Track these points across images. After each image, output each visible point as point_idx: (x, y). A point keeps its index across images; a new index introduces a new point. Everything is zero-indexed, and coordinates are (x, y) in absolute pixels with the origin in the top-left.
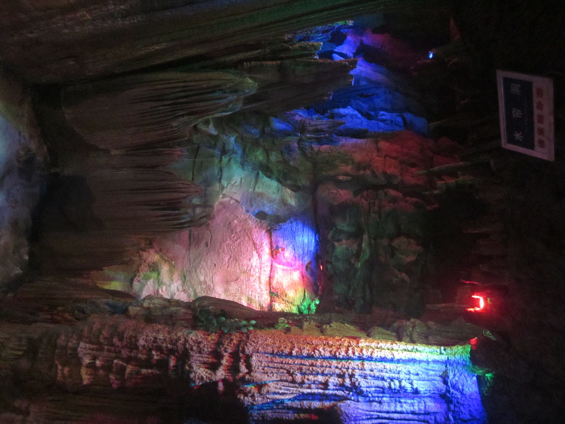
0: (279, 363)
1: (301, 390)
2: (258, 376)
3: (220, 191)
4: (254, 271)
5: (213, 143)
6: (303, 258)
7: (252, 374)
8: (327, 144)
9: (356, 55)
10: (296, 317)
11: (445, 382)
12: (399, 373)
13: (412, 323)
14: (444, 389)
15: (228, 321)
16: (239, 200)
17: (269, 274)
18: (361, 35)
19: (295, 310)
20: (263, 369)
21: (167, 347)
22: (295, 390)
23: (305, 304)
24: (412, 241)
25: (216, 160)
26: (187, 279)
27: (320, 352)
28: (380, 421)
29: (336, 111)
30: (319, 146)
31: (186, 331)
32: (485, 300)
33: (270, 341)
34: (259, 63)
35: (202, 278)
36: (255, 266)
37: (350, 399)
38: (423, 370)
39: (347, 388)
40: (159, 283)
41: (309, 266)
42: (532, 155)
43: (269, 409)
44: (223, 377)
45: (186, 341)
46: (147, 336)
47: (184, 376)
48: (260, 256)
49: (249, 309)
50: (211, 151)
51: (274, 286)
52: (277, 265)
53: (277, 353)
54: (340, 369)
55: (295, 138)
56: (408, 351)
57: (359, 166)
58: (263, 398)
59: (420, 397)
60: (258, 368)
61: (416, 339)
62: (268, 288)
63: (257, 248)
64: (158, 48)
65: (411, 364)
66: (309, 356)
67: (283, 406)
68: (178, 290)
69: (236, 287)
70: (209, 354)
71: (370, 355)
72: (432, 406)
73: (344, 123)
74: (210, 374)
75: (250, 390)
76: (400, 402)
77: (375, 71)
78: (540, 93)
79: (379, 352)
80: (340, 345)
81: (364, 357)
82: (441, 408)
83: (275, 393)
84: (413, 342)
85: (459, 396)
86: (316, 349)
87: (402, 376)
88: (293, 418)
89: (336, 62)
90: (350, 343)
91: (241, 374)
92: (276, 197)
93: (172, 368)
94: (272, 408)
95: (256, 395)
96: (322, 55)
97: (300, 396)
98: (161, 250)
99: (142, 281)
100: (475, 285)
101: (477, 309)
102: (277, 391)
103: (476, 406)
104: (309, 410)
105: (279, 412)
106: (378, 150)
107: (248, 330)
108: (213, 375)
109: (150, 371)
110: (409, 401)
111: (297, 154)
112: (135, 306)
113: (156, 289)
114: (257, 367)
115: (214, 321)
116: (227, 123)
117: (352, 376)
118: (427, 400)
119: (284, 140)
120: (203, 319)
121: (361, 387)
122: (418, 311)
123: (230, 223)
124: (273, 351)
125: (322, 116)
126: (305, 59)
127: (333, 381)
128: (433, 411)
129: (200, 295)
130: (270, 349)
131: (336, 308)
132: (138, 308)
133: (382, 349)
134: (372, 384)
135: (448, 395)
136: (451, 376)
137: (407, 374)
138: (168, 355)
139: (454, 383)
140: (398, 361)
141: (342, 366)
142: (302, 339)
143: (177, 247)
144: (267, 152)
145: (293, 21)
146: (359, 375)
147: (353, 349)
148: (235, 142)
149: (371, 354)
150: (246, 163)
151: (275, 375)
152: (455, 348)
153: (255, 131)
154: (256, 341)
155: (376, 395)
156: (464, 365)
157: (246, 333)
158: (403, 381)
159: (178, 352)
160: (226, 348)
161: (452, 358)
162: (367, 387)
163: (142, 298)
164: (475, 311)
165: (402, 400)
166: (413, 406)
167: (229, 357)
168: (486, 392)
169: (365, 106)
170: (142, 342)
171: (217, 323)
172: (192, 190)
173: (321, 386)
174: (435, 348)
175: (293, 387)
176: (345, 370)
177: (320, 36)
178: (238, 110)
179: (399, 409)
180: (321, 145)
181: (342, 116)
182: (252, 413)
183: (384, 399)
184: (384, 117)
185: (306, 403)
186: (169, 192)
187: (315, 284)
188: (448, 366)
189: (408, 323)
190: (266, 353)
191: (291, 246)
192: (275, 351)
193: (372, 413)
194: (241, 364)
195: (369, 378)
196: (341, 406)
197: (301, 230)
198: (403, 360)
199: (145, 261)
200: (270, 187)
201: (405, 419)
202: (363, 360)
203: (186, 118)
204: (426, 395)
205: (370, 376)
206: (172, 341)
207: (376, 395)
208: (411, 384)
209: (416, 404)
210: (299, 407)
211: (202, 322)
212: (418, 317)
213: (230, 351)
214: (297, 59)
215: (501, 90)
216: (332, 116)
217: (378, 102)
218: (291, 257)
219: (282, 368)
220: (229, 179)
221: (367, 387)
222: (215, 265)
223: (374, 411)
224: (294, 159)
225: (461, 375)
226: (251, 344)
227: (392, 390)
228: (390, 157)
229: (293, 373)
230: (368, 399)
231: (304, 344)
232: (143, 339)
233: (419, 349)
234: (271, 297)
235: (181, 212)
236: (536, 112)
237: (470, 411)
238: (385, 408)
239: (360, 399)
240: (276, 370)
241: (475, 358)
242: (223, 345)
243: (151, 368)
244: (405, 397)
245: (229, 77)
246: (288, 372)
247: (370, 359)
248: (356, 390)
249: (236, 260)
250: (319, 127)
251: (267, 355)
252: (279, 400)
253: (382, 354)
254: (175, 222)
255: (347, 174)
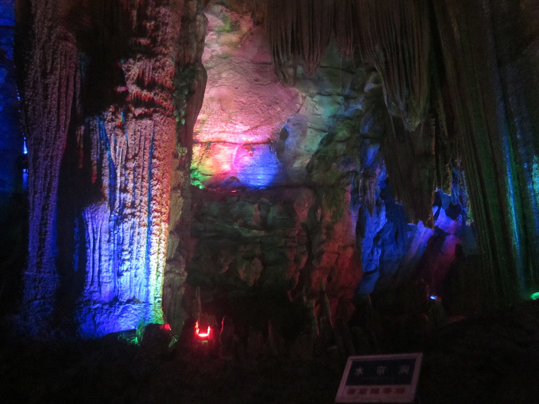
0: (144, 146)
1: (119, 167)
2: (132, 126)
3: (309, 94)
4: (231, 127)
5: (356, 87)
6: (243, 174)
7: (134, 120)
8: (352, 199)
9: (437, 229)
10: (187, 165)
11: (129, 301)
12: (136, 259)
13: (183, 273)
14: (123, 300)
15: (184, 97)
16: (300, 112)
17: (228, 141)
18: (455, 234)
19: (194, 165)
20: (138, 131)
21: (158, 36)
22: (119, 161)
23: (199, 176)
24: (258, 277)
25: (339, 90)
26: (224, 60)
27: (155, 186)
28: (92, 241)
29: (384, 208)
30: (350, 191)
31: (174, 55)
32: (206, 338)
33: (165, 137)
34: (434, 134)
35: (224, 75)
36: (235, 128)
37: (111, 213)
38: (140, 282)
39: (121, 211)
40: (220, 31)
41: (235, 180)
42: (341, 381)
43: (100, 136)
44: (130, 91)
45: (165, 55)
46: (169, 16)
47: (130, 53)
48: (245, 132)
49: (194, 121)
50: (349, 85)
51: (216, 146)
52: (237, 148)
53: (154, 144)
54: (140, 204)
55: (359, 169)
56: (157, 268)
57: (330, 228)
58: (111, 130)
59: (114, 278)
60: (139, 126)
61: (168, 276)
62: (214, 140)
63: (253, 130)
64: (455, 30)
65: (145, 271)
66: (151, 175)
67: (103, 149)
68: (213, 51)
69: (216, 109)
70: (152, 77)
71: (153, 232)
72: (107, 289)
73: (371, 216)
74: (133, 79)
75: (118, 118)
76: (110, 260)
77: (420, 246)
78: (402, 391)
79: (156, 241)
80: (162, 205)
81: (151, 227)
82: (105, 297)
83: (116, 141)
84: (166, 273)
85: (116, 314)
86: (158, 182)
87: (134, 262)
88: (92, 159)
89: (431, 208)
90: (165, 214)
91: (133, 108)
92: (302, 148)
93: (138, 42)
94: (101, 139)
95: (114, 123)
96: (438, 195)
97: (114, 165)
98: (252, 34)
99: (221, 14)
100: (220, 330)
101: (198, 331)
102: (118, 144)
103: (108, 328)
104: (100, 175)
105: (97, 146)
106: (345, 247)
107: (175, 117)
108: (132, 82)
109: (135, 18)
110: (110, 268)
111: (342, 170)
112: (197, 7)
113: (214, 29)
114: (140, 124)
115: (184, 84)
116: (376, 101)
117: (133, 215)
118: (112, 285)
119: (357, 157)
120: (186, 72)
121: (123, 223)
122: (192, 282)
123: (278, 103)
124: (156, 140)
125: (378, 195)
126: (435, 179)
127: (129, 198)
128: (102, 289)
129: (208, 73)
130: (157, 137)
131: (195, 205)
132: (195, 10)
133: (159, 244)
134: (126, 234)
135: (118, 303)
136: (134, 307)
137: (136, 266)
138: (150, 37)
139: (129, 310)
140: (148, 259)
141: (142, 206)
142: (167, 169)
143: (255, 50)
144: (346, 141)
145: (475, 166)
146: (134, 222)
147: (159, 217)
148: (357, 109)
149: (154, 234)
150: (335, 119)
151: (133, 142)
152: (160, 311)
153: (366, 129)
154: (165, 124)
155: (116, 238)
156: (145, 319)
157: (173, 114)
158: (129, 263)
159: (153, 47)
160: (158, 94)
161: (151, 308)
162: (123, 229)
163: (205, 14)
164: (196, 329)
165: (111, 262)
166: (107, 272)
167: (150, 98)
168: (121, 338)
169: (387, 235)
170: (163, 10)
171: (182, 87)
172: (311, 65)
173: (123, 186)
174: (161, 292)
175: (122, 159)
176: (139, 209)
177: (457, 193)
178: (389, 111)
179: (103, 258)
180: (351, 193)
181: (378, 213)
182: (96, 119)
183: (112, 245)
184: (376, 253)
185: (107, 171)
186: (310, 42)
187: (218, 186)
188: (144, 304)
189: (183, 269)
190: (154, 133)
191: (254, 163)
192: (155, 142)
193: (99, 234)
194: (143, 109)
195: (132, 231)
196: (105, 204)
197: (270, 173)
198: (149, 263)
199: (241, 17)
200: (311, 143)
201: (94, 264)
202: (149, 226)
203: (382, 59)
204: (117, 283)
205: (134, 233)
206: (165, 41)
207: (116, 238)
208: (127, 270)
209: (108, 275)
210: (103, 165)
211: (183, 71)
212: (188, 281)
213: (156, 98)
214: (436, 171)
215: (404, 356)
216: (378, 204)
217: (390, 248)
218: (244, 163)
219: (140, 148)
220: (320, 103)
221: (123, 229)
222: (237, 88)
223: (100, 235)
224: (338, 167)
225: (136, 315)
226: (162, 119)
227: (121, 252)
228: (337, 258)
229: (135, 159)
230: (112, 230)
231: (163, 170)
232: (166, 12)
233: (159, 278)
234: (206, 143)
235: (290, 53)
236: (382, 388)
237: (103, 323)
238: (104, 246)
239: (112, 223)
240: (138, 143)
241: (151, 329)
242: (161, 92)
243: (137, 20)
244: (114, 265)
245: (422, 104)
246: (136, 155)
247: (150, 233)
248: (120, 219)
249: (242, 109)
250: (368, 191)
251: (152, 134)
252: (109, 145)
253: (154, 244)
254: (280, 48)
255: (322, 217)
